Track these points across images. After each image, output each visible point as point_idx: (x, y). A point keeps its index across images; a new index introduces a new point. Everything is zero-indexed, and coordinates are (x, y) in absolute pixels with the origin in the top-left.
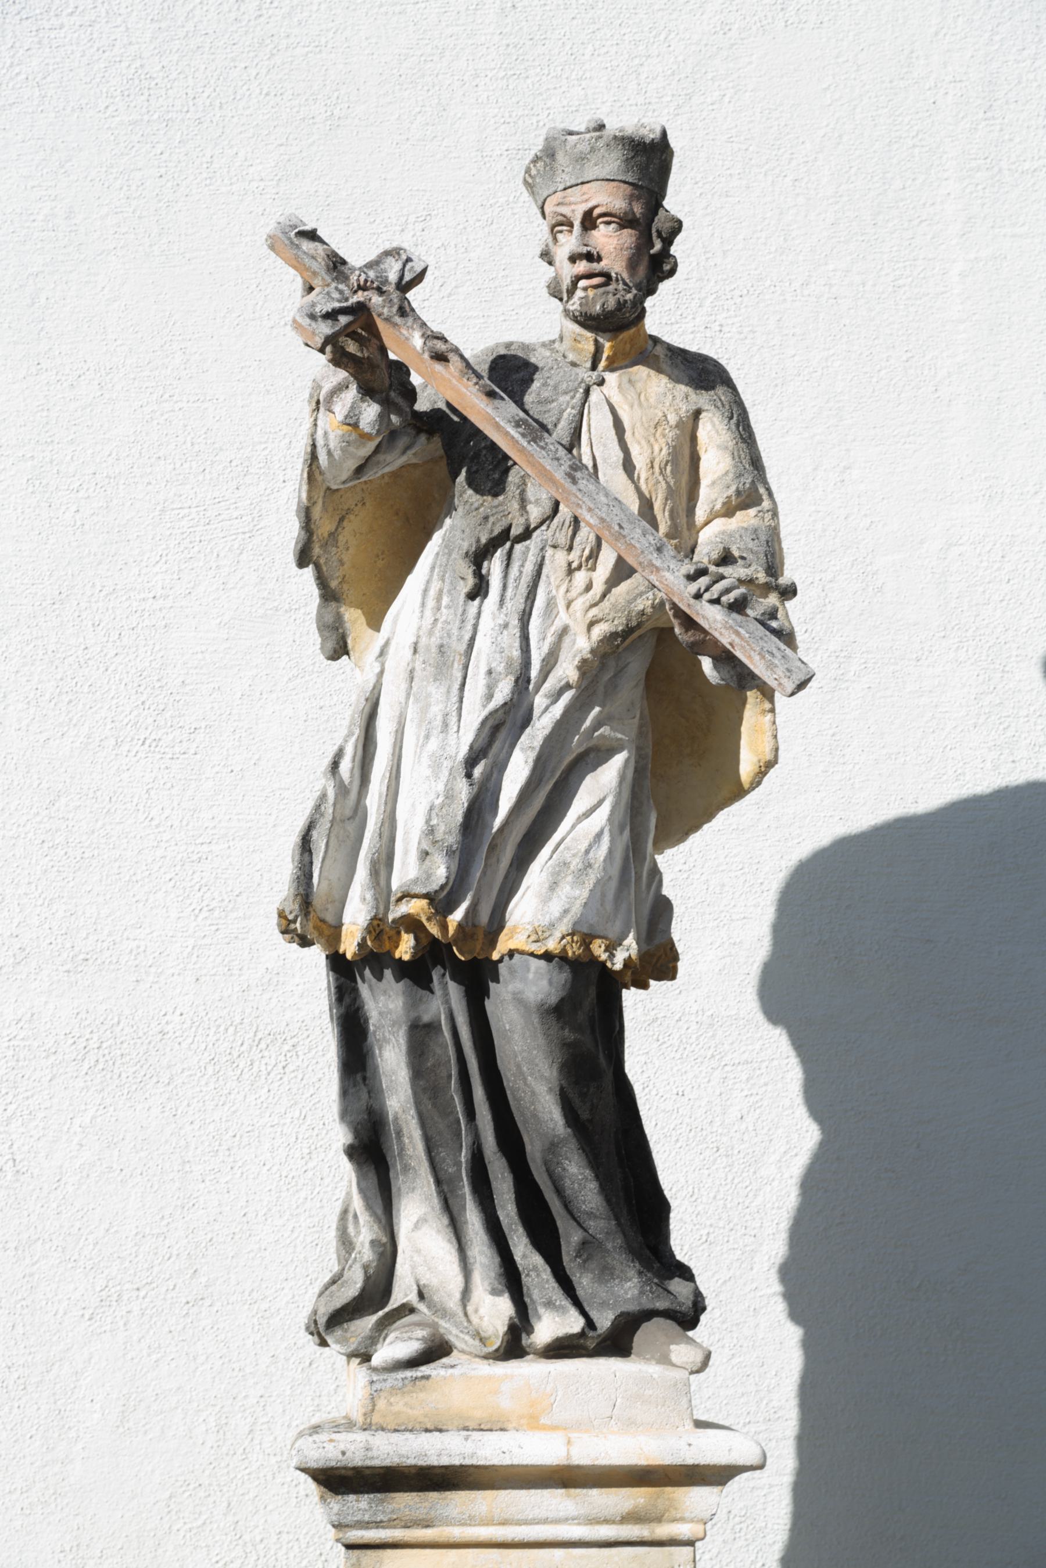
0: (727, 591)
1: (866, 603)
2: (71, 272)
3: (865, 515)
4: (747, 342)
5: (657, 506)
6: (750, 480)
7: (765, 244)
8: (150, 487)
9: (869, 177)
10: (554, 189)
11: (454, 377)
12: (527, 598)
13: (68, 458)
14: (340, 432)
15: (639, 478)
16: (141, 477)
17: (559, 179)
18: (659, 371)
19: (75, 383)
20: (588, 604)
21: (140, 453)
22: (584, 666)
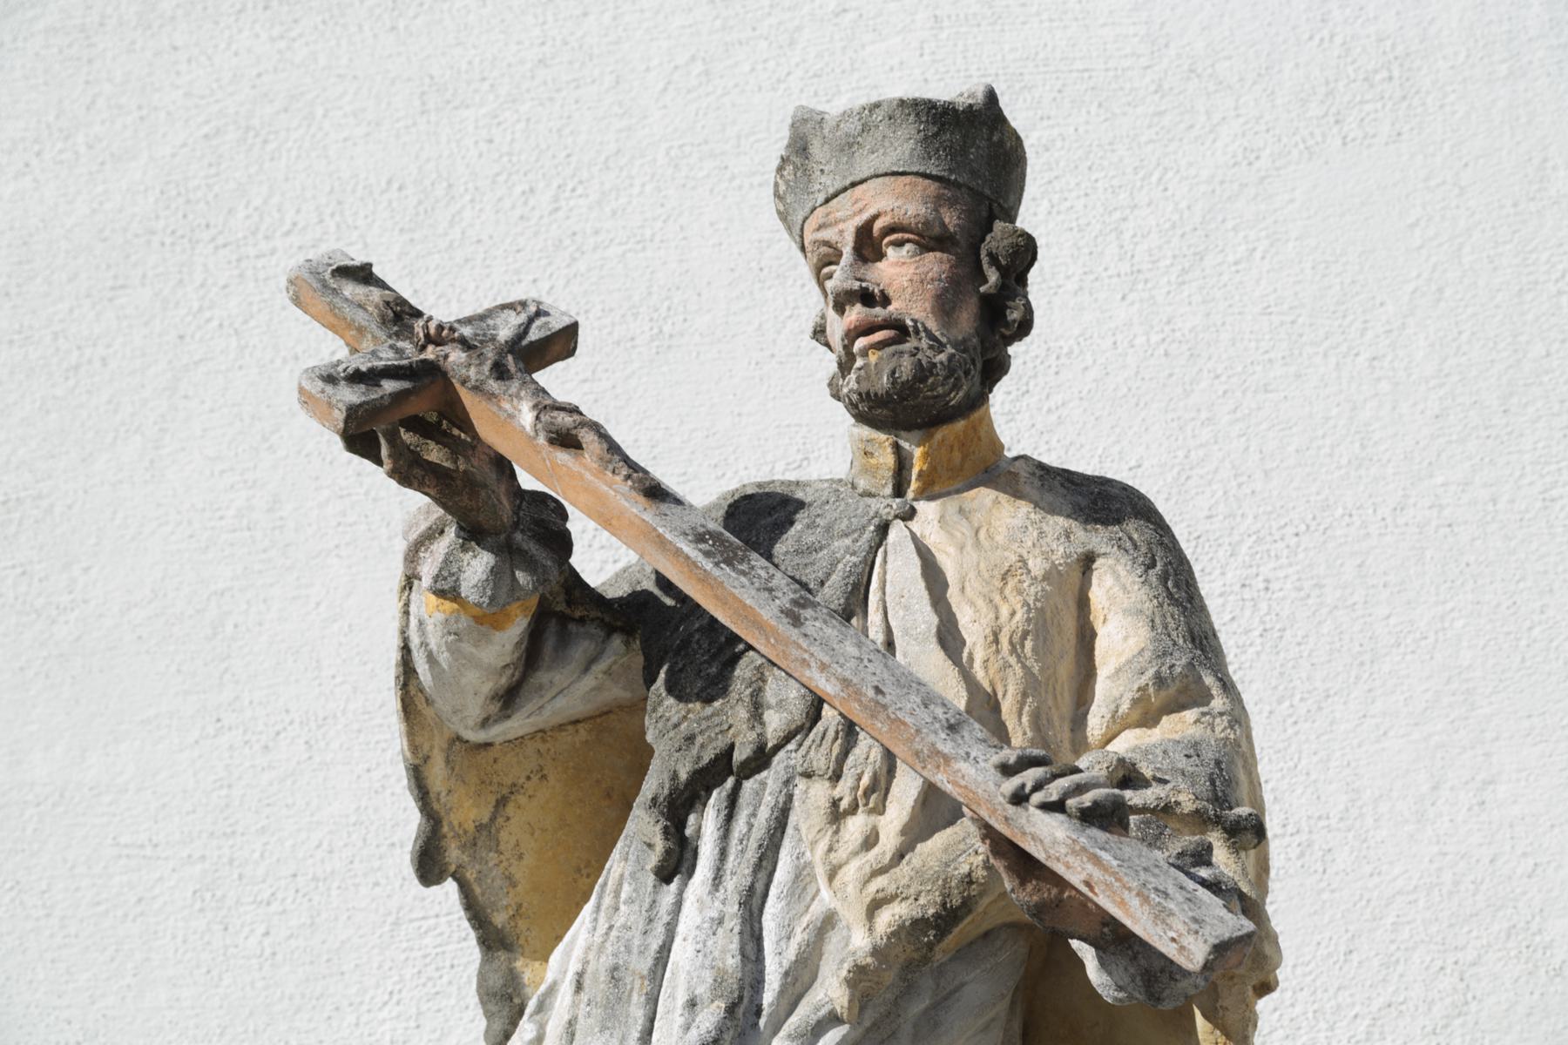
0: (1080, 789)
1: (1536, 996)
2: (271, 585)
3: (1525, 854)
4: (1310, 602)
5: (1007, 706)
6: (1184, 661)
7: (1331, 455)
8: (378, 890)
9: (1491, 344)
10: (810, 205)
11: (590, 470)
12: (758, 867)
13: (257, 855)
14: (440, 617)
15: (971, 658)
16: (365, 875)
17: (817, 187)
18: (1017, 495)
19: (271, 744)
20: (867, 870)
21: (365, 840)
22: (859, 978)
